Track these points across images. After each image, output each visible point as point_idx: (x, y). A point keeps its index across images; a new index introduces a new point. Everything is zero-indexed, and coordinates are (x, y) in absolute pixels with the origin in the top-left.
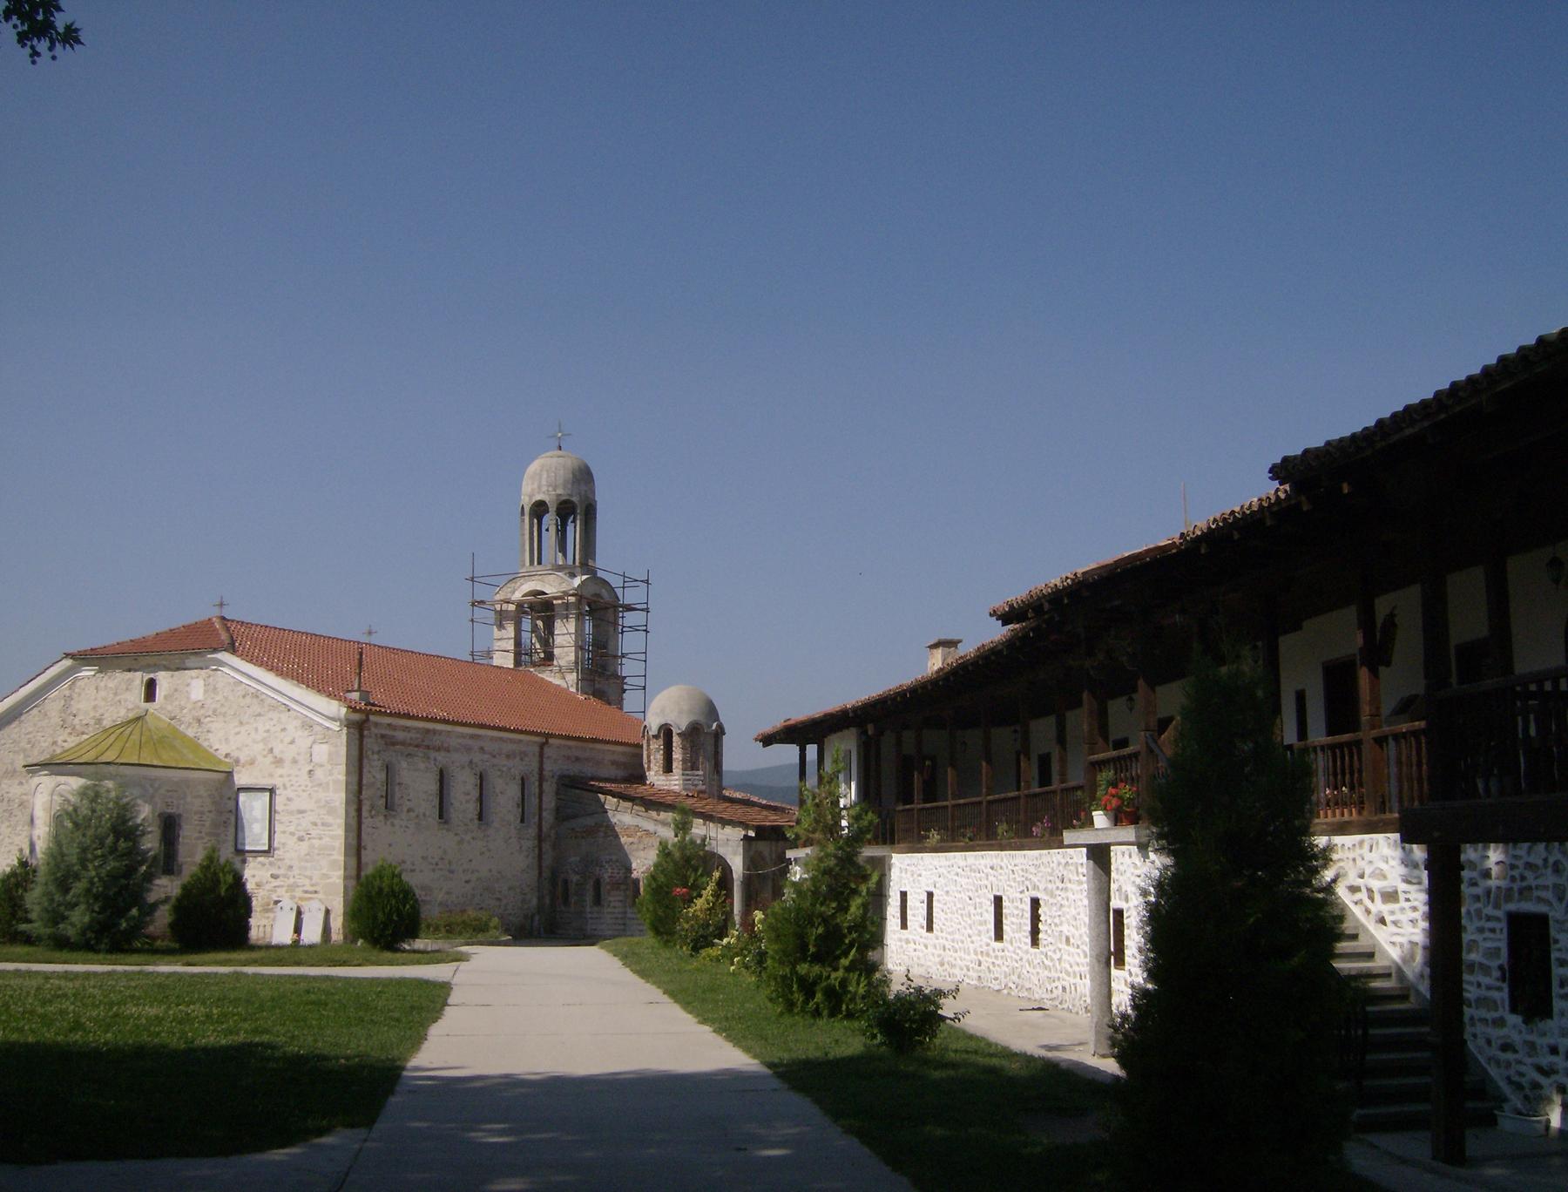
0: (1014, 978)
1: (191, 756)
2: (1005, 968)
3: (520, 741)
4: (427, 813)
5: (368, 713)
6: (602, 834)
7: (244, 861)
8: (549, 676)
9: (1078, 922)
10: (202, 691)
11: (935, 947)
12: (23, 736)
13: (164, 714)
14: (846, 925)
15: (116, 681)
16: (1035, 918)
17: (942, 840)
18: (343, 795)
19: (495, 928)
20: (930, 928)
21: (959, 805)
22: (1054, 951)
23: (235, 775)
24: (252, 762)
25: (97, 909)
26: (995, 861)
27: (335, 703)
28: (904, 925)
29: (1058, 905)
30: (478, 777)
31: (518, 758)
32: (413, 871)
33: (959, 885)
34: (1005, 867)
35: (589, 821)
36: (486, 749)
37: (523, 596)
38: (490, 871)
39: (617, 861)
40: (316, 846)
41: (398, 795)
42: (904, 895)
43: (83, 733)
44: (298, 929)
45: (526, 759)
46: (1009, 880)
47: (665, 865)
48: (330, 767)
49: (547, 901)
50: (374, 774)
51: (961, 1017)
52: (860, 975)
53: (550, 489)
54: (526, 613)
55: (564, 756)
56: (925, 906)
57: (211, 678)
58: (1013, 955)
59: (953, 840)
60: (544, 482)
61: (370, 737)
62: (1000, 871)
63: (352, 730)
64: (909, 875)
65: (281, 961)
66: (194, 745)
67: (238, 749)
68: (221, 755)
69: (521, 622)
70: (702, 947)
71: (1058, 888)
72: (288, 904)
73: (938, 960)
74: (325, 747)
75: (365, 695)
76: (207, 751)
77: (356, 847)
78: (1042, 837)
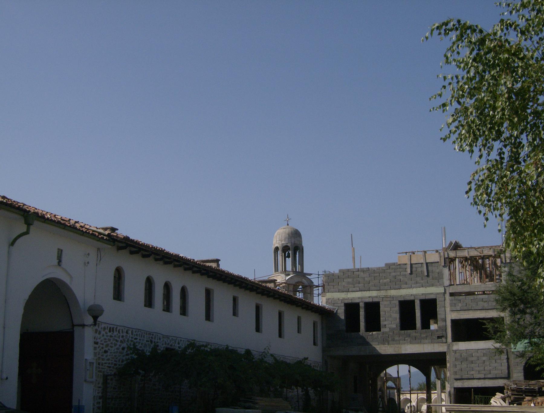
53: (280, 242)
60: (278, 240)
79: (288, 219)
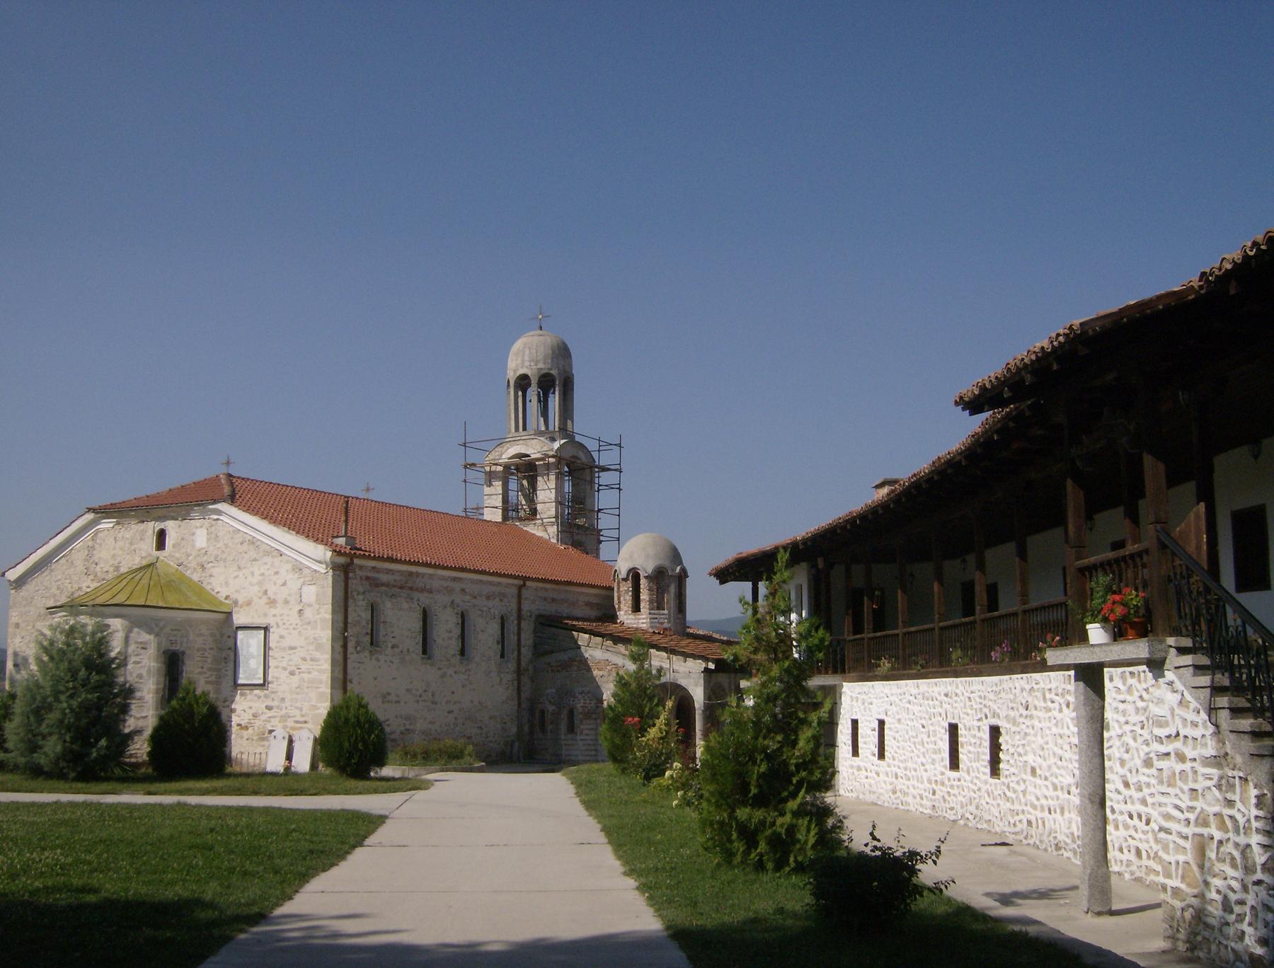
0: (972, 808)
1: (194, 598)
2: (960, 798)
3: (499, 584)
4: (411, 650)
5: (352, 557)
6: (575, 668)
8: (533, 529)
9: (1047, 752)
10: (205, 539)
11: (887, 774)
12: (53, 583)
14: (793, 761)
16: (995, 748)
17: (893, 668)
19: (470, 755)
20: (881, 755)
21: (911, 633)
22: (1018, 783)
24: (249, 603)
25: (68, 738)
26: (949, 688)
27: (321, 548)
28: (855, 752)
29: (1022, 734)
31: (498, 599)
32: (398, 702)
33: (911, 713)
34: (960, 694)
35: (564, 656)
36: (467, 590)
40: (306, 680)
41: (382, 632)
42: (855, 723)
44: (289, 757)
46: (965, 708)
47: (622, 695)
49: (526, 728)
50: (359, 613)
51: (943, 887)
52: (810, 821)
53: (532, 364)
54: (512, 474)
55: (541, 597)
56: (876, 733)
57: (213, 528)
58: (970, 785)
59: (904, 669)
60: (526, 358)
61: (356, 578)
62: (956, 698)
63: (338, 573)
64: (860, 703)
65: (239, 790)
66: (199, 589)
68: (222, 597)
70: (655, 776)
71: (1021, 715)
72: (280, 733)
73: (890, 787)
75: (351, 540)
77: (342, 678)
78: (1001, 662)
79: (540, 316)
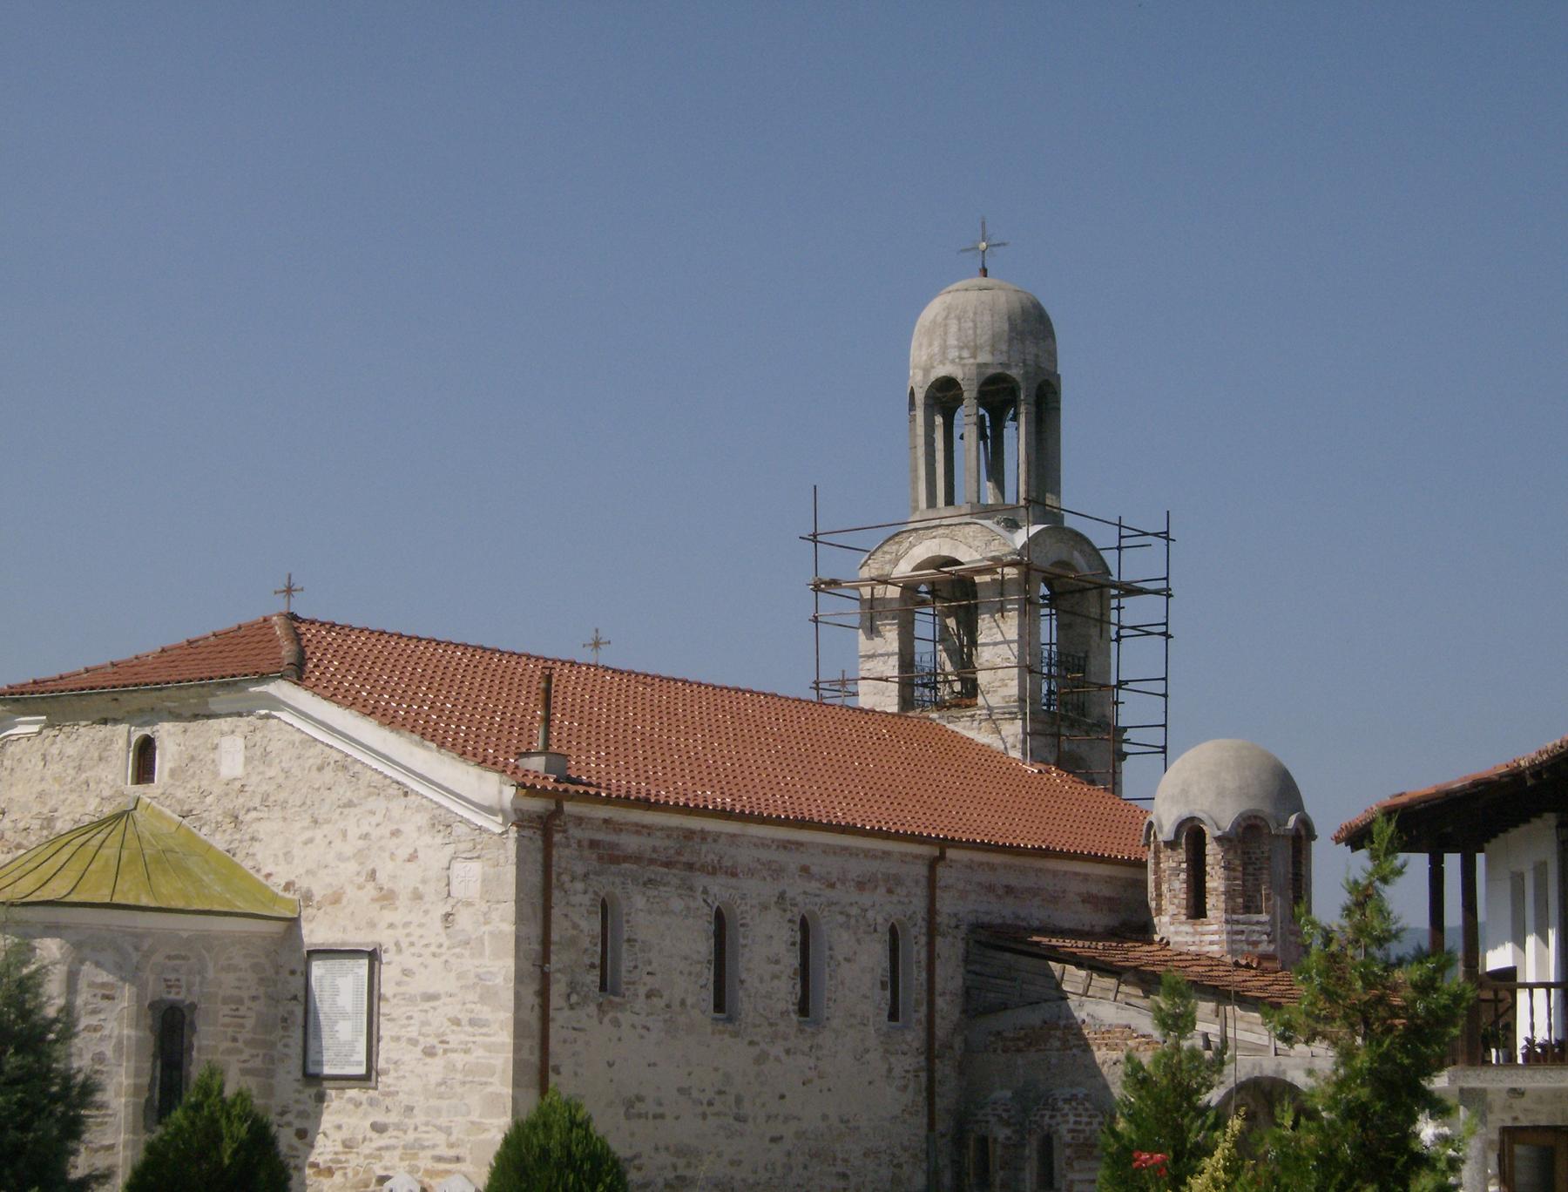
3: (886, 854)
4: (689, 1002)
7: (321, 1098)
10: (240, 759)
13: (169, 806)
15: (79, 742)
18: (509, 963)
23: (303, 924)
27: (493, 778)
30: (797, 927)
31: (882, 890)
35: (1033, 1017)
36: (814, 869)
37: (915, 569)
38: (825, 1117)
39: (1087, 1097)
41: (626, 963)
43: (19, 846)
45: (899, 890)
48: (484, 907)
53: (965, 354)
54: (923, 603)
57: (259, 734)
60: (952, 341)
61: (568, 846)
66: (227, 867)
67: (308, 872)
69: (913, 622)
74: (476, 867)
75: (557, 762)
76: (247, 876)
